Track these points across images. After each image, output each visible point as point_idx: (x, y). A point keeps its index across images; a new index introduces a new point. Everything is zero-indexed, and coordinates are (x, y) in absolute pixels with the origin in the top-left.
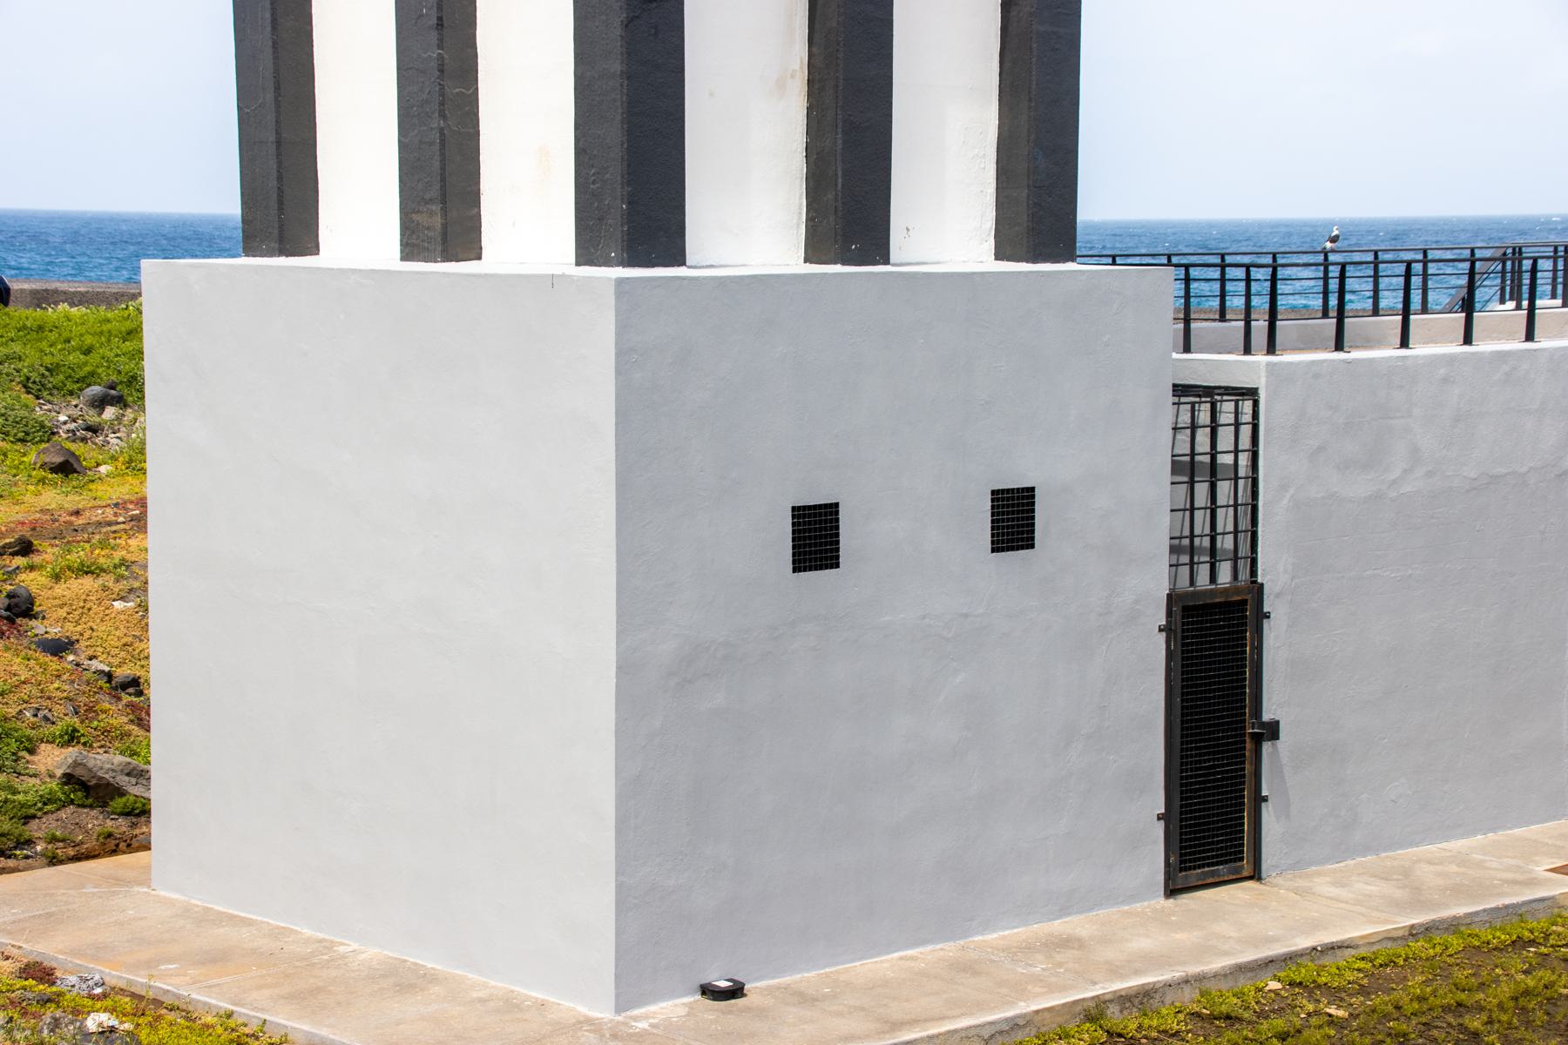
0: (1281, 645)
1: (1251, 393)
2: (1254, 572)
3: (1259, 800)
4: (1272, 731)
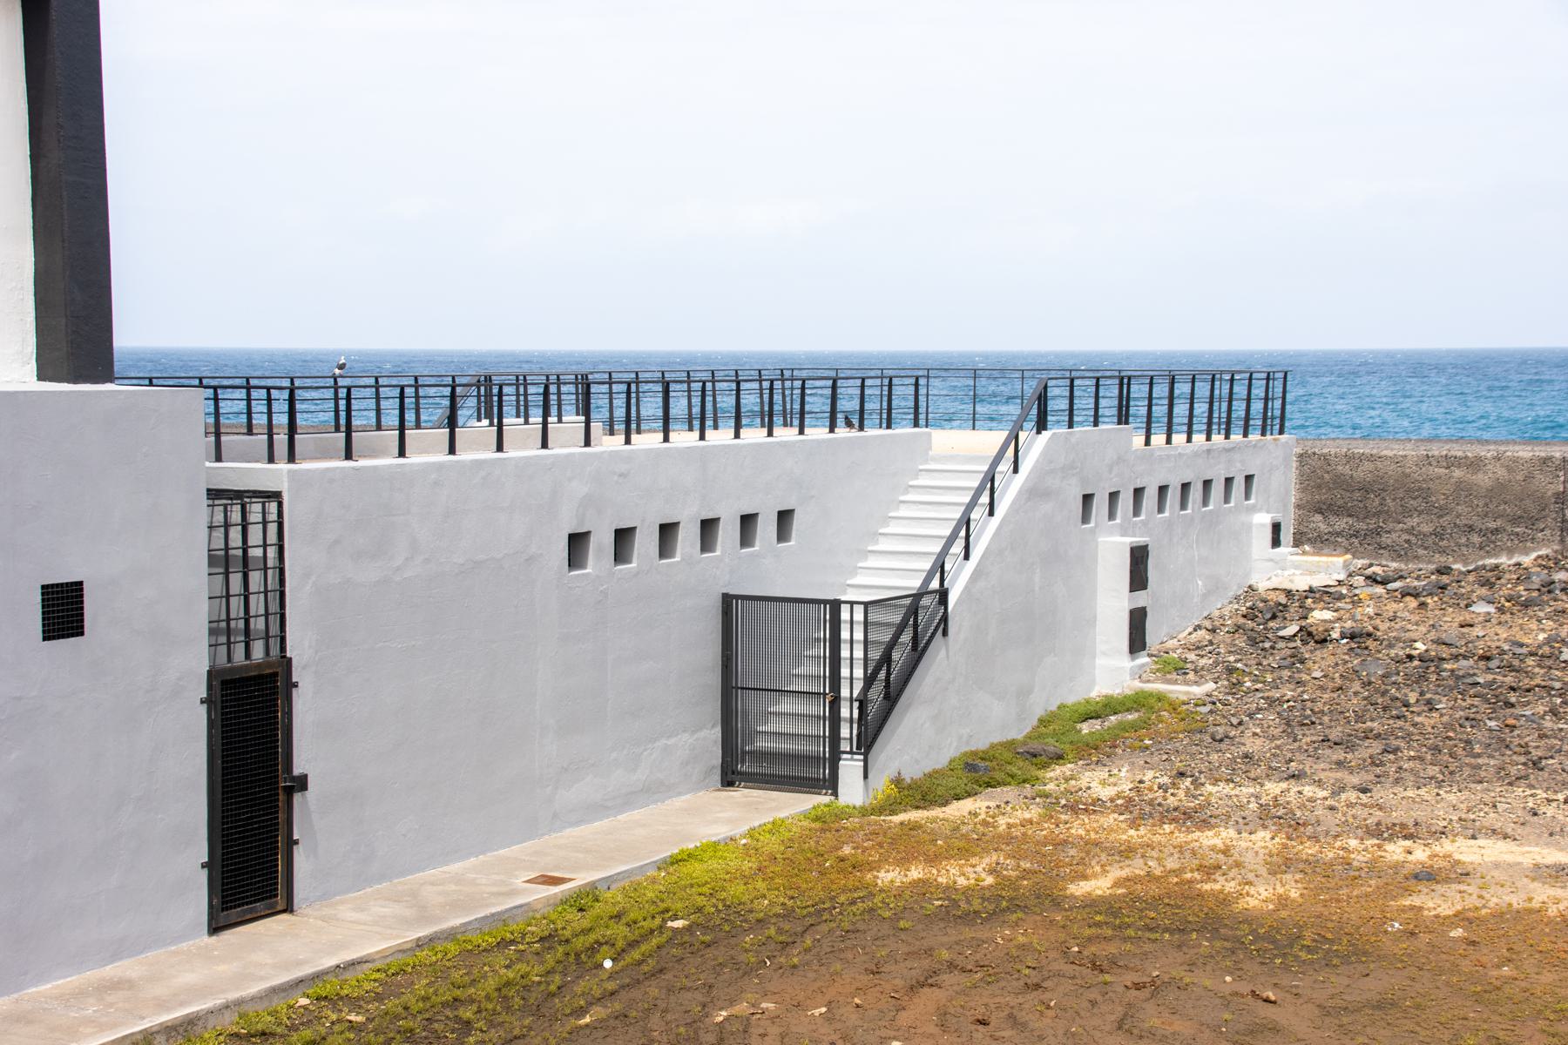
0: (309, 712)
1: (276, 496)
2: (283, 648)
3: (291, 843)
4: (302, 783)
